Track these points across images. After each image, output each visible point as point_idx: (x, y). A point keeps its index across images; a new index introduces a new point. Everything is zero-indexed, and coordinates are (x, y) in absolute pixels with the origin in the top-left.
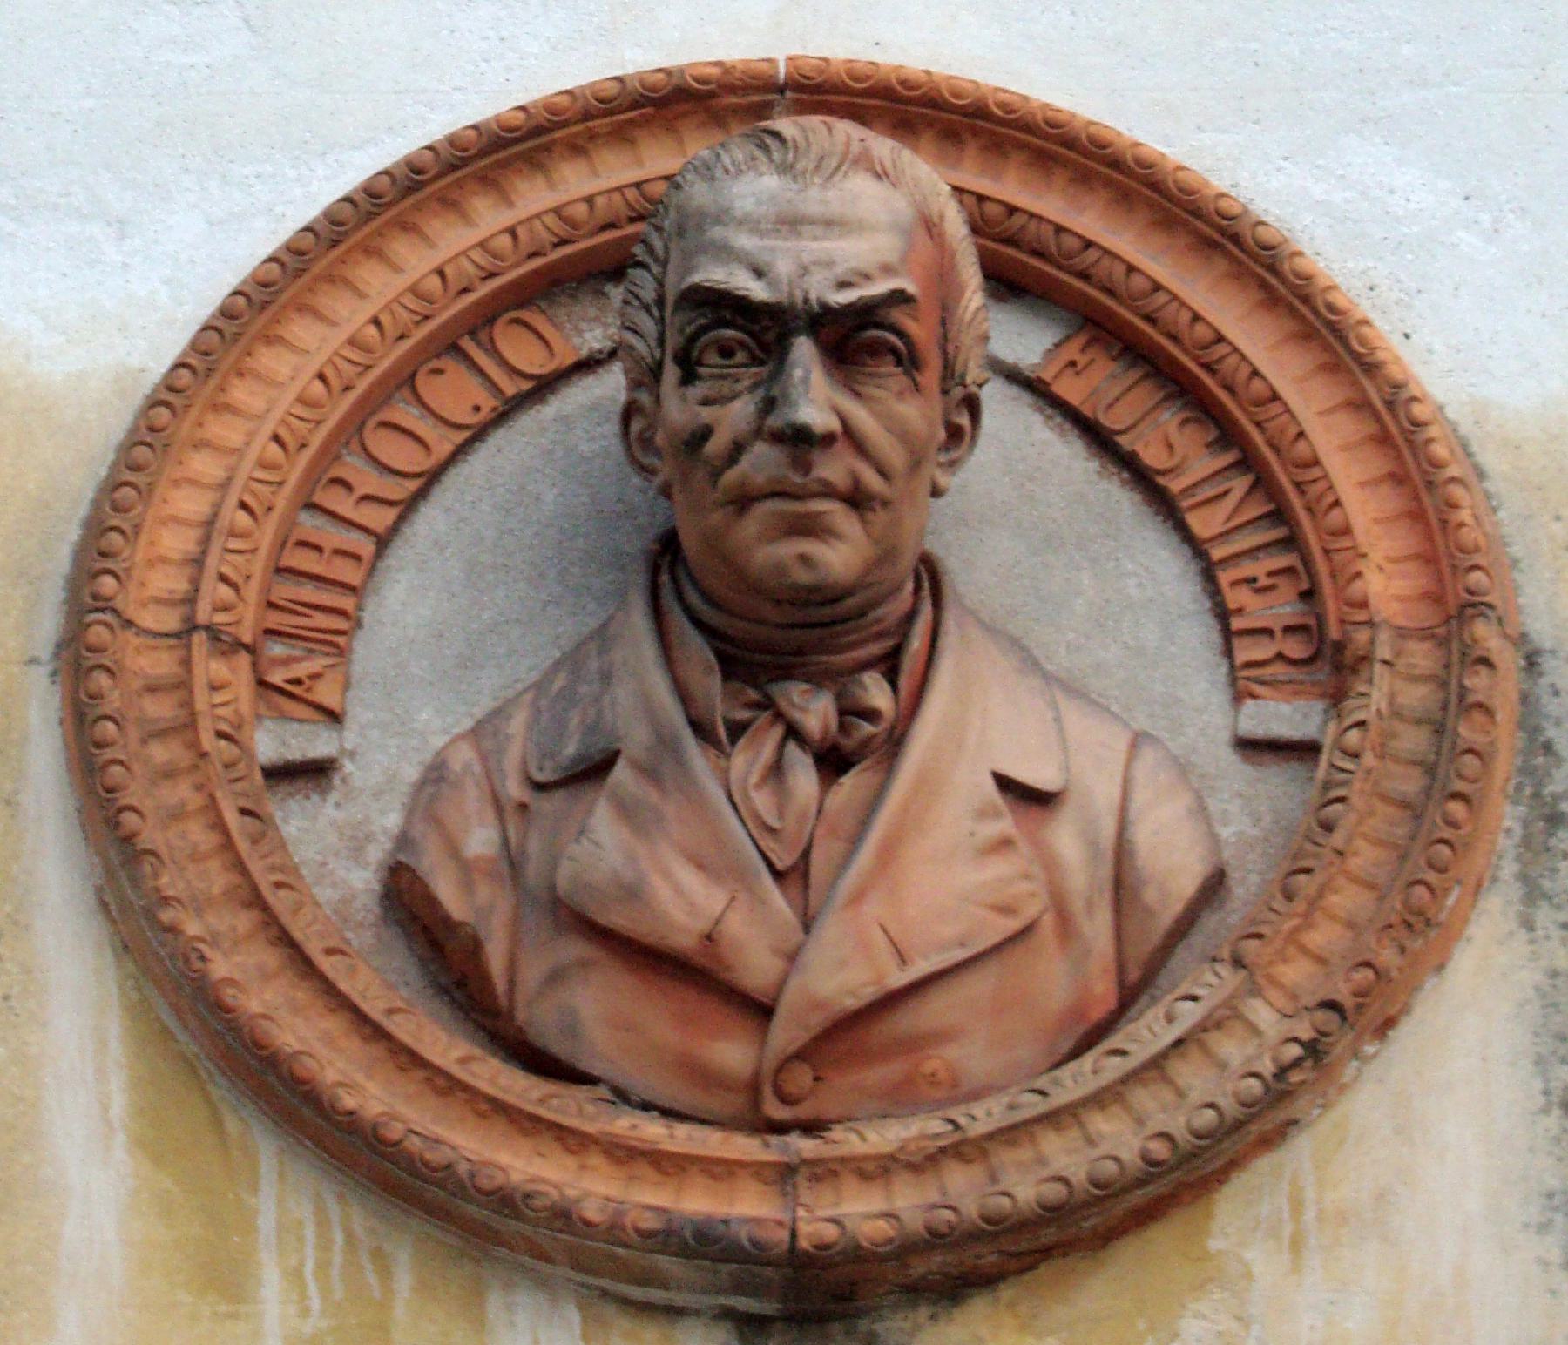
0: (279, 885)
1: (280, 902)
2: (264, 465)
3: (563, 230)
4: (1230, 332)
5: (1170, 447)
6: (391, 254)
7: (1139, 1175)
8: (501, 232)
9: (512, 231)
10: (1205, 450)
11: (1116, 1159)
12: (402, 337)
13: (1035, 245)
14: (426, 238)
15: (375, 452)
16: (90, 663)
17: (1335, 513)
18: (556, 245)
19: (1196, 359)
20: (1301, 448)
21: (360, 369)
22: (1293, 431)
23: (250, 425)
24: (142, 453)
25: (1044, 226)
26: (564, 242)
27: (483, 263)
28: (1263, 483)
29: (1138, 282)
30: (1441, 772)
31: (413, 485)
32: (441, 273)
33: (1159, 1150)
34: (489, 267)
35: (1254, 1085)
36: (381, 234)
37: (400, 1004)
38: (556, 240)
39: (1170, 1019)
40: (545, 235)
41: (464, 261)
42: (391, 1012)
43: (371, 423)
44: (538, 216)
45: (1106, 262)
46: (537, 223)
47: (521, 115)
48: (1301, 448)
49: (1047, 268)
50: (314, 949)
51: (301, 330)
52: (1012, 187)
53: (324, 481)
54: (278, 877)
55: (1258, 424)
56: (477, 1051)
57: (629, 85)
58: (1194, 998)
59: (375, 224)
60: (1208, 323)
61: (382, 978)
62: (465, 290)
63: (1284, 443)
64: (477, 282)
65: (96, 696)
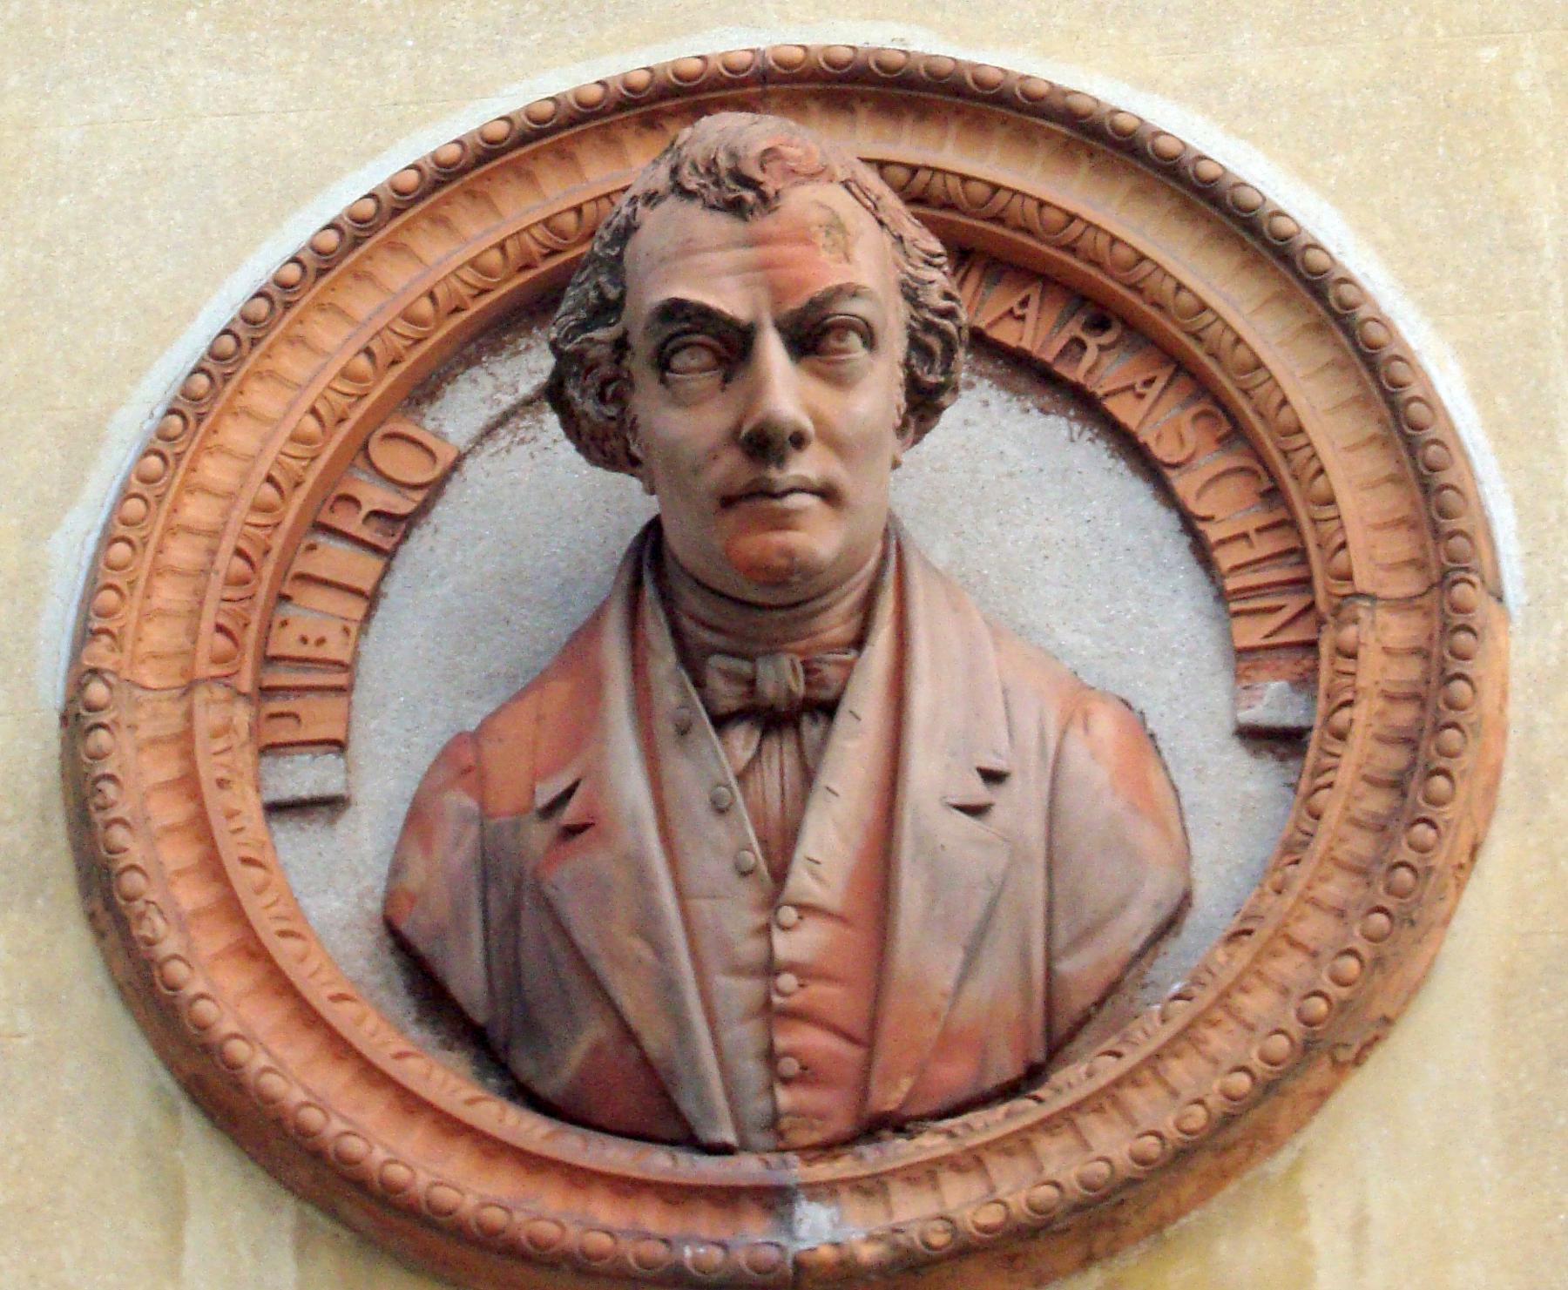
0: (283, 934)
1: (284, 952)
2: (257, 508)
3: (554, 242)
4: (1214, 300)
5: (1182, 441)
6: (416, 250)
7: (1129, 1174)
8: (491, 247)
9: (501, 247)
10: (1215, 447)
11: (1107, 1160)
12: (394, 363)
13: (1091, 255)
14: (492, 207)
15: (381, 465)
16: (91, 721)
17: (1285, 412)
18: (546, 256)
19: (1182, 328)
20: (1285, 416)
21: (409, 342)
22: (1276, 399)
23: (291, 394)
24: (134, 507)
25: (1028, 202)
26: (554, 252)
27: (471, 280)
28: (1273, 494)
29: (1122, 253)
30: (1423, 744)
31: (419, 496)
32: (431, 295)
33: (1150, 1146)
34: (480, 285)
35: (1241, 1082)
36: (370, 258)
37: (410, 1049)
38: (545, 251)
39: (1164, 1020)
40: (534, 247)
41: (453, 280)
42: (400, 1056)
43: (379, 433)
44: (527, 229)
45: (938, 178)
46: (526, 236)
47: (698, 64)
48: (1285, 416)
49: (1031, 242)
50: (318, 996)
51: (292, 363)
52: (915, 145)
53: (302, 547)
54: (284, 926)
55: (1245, 392)
56: (479, 1093)
57: (812, 55)
58: (1118, 1055)
59: (362, 249)
60: (1190, 291)
61: (385, 1027)
62: (457, 310)
63: (1272, 412)
64: (469, 301)
65: (99, 756)
